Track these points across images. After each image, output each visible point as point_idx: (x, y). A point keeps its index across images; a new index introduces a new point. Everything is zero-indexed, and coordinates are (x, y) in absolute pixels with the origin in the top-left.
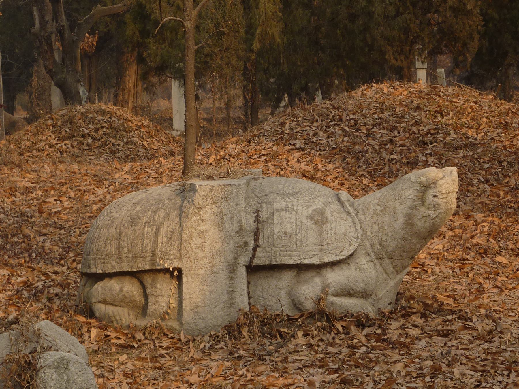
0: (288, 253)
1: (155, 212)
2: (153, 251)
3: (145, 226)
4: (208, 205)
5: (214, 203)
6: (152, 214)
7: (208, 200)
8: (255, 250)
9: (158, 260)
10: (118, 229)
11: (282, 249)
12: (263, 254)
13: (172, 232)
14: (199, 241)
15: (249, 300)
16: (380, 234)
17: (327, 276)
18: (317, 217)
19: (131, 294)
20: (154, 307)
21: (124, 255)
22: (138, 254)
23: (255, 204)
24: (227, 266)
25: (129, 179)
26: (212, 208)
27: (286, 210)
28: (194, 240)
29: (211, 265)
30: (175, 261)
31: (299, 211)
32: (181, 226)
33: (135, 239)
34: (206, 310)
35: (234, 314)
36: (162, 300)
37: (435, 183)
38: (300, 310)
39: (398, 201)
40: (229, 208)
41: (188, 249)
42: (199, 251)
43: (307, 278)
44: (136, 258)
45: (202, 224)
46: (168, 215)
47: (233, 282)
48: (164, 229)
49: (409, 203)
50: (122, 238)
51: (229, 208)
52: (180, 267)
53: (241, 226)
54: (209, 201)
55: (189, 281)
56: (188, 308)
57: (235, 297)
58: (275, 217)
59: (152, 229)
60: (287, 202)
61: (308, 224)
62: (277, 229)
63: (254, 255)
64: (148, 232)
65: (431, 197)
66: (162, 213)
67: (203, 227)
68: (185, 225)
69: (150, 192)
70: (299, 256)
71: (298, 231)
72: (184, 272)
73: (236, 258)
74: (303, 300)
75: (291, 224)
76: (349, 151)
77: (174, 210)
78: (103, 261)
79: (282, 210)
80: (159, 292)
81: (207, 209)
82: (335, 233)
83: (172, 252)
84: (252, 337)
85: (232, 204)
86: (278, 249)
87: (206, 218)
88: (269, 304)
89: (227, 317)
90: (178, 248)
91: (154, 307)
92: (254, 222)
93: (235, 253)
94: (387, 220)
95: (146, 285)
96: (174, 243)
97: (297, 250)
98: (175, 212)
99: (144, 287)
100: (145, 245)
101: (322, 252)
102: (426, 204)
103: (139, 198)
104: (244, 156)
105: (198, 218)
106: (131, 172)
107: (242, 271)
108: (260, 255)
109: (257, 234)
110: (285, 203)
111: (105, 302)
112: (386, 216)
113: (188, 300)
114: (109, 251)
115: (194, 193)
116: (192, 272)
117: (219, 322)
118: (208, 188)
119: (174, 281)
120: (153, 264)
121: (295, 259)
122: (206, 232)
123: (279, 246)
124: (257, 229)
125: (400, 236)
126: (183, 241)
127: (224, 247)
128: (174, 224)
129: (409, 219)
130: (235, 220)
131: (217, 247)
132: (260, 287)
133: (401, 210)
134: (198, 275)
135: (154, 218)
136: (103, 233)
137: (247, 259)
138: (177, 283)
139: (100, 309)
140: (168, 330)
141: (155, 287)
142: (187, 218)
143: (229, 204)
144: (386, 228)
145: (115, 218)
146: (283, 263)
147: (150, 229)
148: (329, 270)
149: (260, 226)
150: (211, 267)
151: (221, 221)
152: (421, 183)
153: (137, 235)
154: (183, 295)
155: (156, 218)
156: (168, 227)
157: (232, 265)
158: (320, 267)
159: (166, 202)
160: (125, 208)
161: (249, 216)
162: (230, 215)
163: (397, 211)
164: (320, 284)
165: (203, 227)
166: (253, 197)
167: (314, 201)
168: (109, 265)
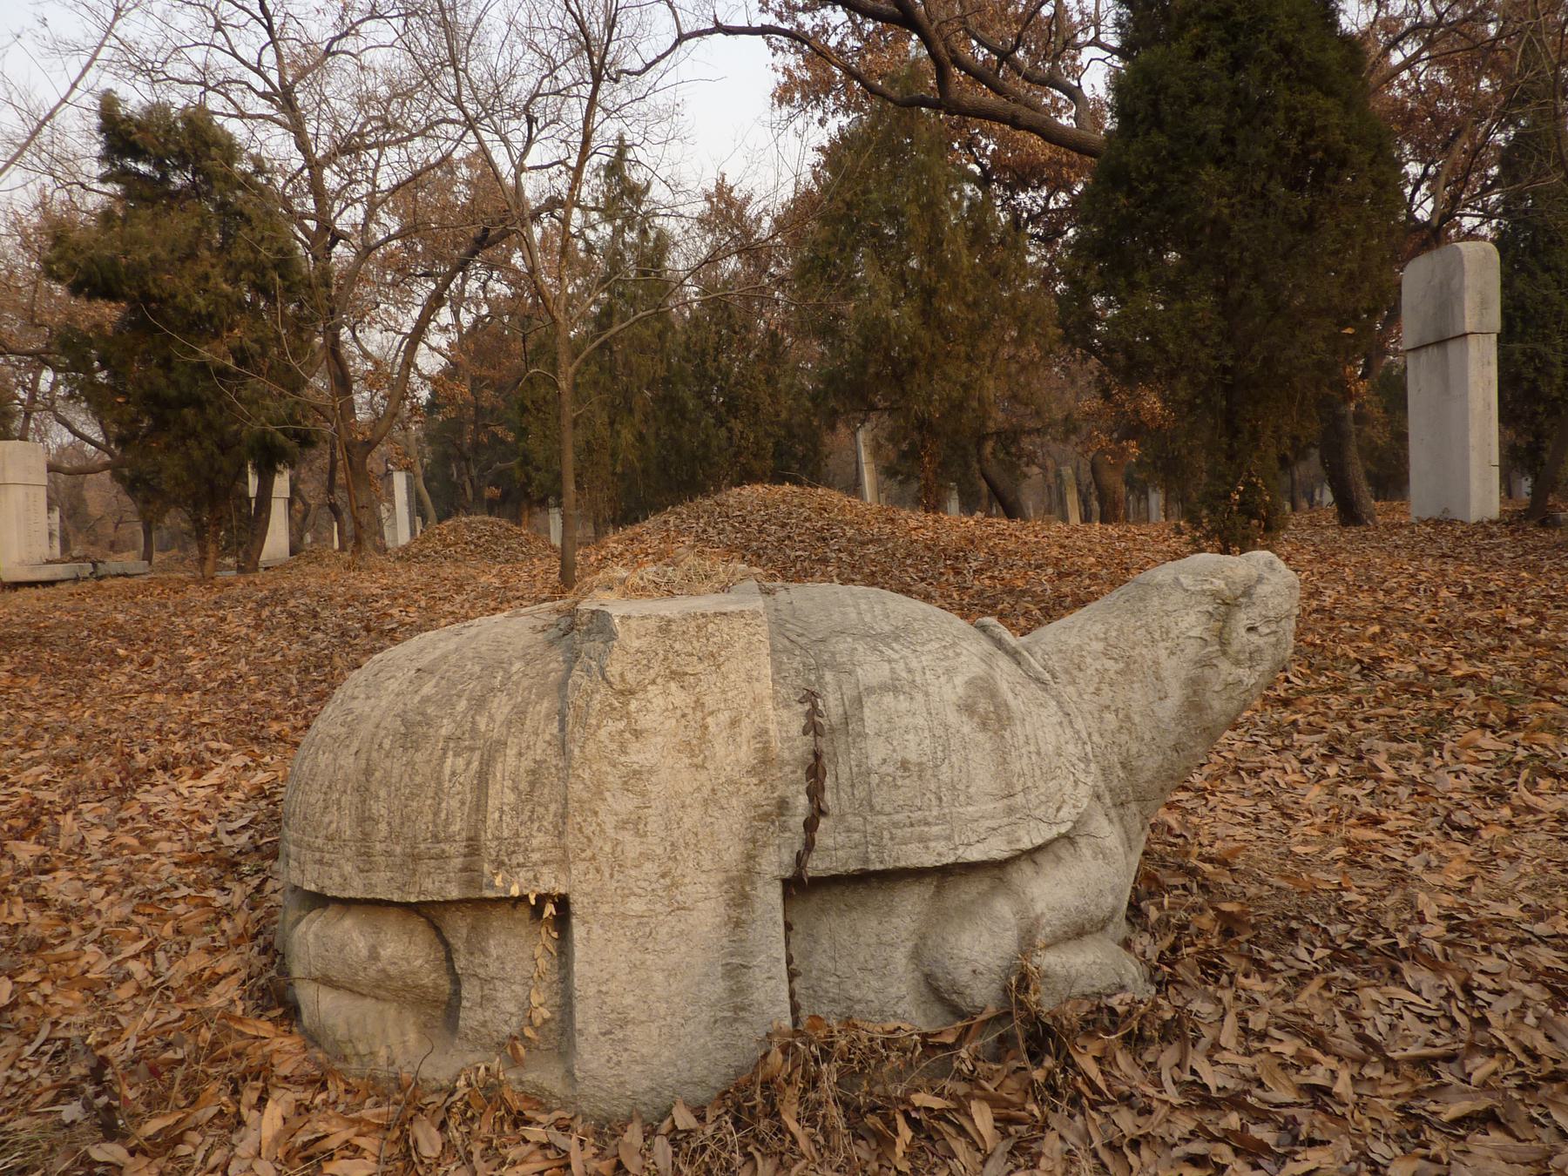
0: (917, 829)
1: (479, 703)
2: (470, 839)
3: (445, 750)
4: (653, 682)
5: (675, 675)
6: (469, 708)
7: (655, 664)
8: (810, 826)
9: (487, 868)
10: (363, 756)
11: (896, 817)
12: (839, 839)
13: (533, 772)
14: (625, 804)
15: (790, 982)
16: (1124, 738)
17: (1030, 895)
18: (983, 705)
19: (405, 967)
20: (479, 1015)
21: (379, 847)
22: (422, 846)
23: (797, 672)
24: (721, 884)
25: (497, 583)
26: (666, 693)
27: (893, 687)
28: (610, 799)
29: (668, 881)
30: (545, 870)
31: (931, 689)
32: (563, 749)
33: (413, 796)
34: (655, 1033)
35: (748, 1036)
36: (507, 994)
37: (1247, 592)
38: (957, 1012)
39: (1161, 644)
40: (724, 692)
41: (588, 831)
42: (627, 836)
43: (966, 897)
44: (416, 858)
45: (634, 746)
46: (520, 713)
47: (743, 935)
48: (508, 763)
49: (1192, 649)
50: (372, 789)
51: (724, 692)
52: (563, 891)
53: (766, 748)
54: (656, 667)
55: (594, 936)
56: (594, 1029)
57: (750, 986)
58: (867, 712)
59: (468, 764)
60: (890, 662)
61: (966, 729)
62: (876, 751)
63: (809, 845)
64: (453, 774)
65: (1243, 631)
66: (501, 707)
67: (639, 756)
68: (577, 751)
69: (473, 631)
70: (949, 838)
71: (940, 754)
72: (576, 908)
73: (750, 857)
74: (965, 979)
75: (917, 733)
76: (746, 548)
77: (541, 697)
78: (318, 855)
79: (884, 688)
80: (493, 968)
81: (650, 695)
82: (1038, 753)
83: (535, 842)
84: (820, 1138)
85: (732, 677)
86: (884, 819)
87: (649, 725)
88: (856, 994)
89: (726, 1053)
90: (556, 827)
91: (479, 1015)
92: (805, 733)
93: (746, 841)
94: (1138, 697)
95: (451, 940)
96: (541, 810)
97: (942, 819)
98: (546, 704)
99: (449, 951)
100: (443, 816)
101: (1013, 819)
102: (1232, 650)
103: (438, 653)
104: (628, 556)
105: (621, 725)
106: (499, 575)
107: (770, 896)
108: (830, 842)
109: (815, 772)
110: (886, 666)
111: (327, 981)
112: (1135, 686)
113: (591, 1002)
114: (334, 826)
115: (606, 642)
116: (606, 909)
117: (699, 1071)
118: (652, 624)
119: (543, 930)
120: (471, 883)
121: (939, 849)
122: (651, 771)
123: (888, 809)
124: (817, 756)
125: (1171, 740)
126: (573, 805)
127: (709, 820)
128: (541, 745)
129: (1195, 692)
130: (747, 730)
131: (687, 823)
132: (825, 942)
133: (1175, 671)
134: (624, 916)
135: (474, 723)
136: (323, 766)
137: (788, 857)
138: (555, 935)
139: (320, 1004)
140: (527, 1098)
141: (484, 952)
142: (585, 726)
143: (725, 678)
144: (1137, 719)
145: (360, 719)
146: (902, 864)
147: (461, 762)
148: (1027, 868)
149: (824, 745)
150: (667, 888)
151: (698, 734)
152: (1215, 595)
153: (418, 779)
154: (577, 983)
155: (482, 723)
156: (520, 754)
157: (741, 880)
158: (995, 869)
159: (517, 666)
160: (393, 685)
161: (785, 714)
162: (727, 714)
163: (1164, 674)
164: (1013, 921)
165: (639, 756)
166: (785, 650)
167: (958, 655)
168: (335, 872)
